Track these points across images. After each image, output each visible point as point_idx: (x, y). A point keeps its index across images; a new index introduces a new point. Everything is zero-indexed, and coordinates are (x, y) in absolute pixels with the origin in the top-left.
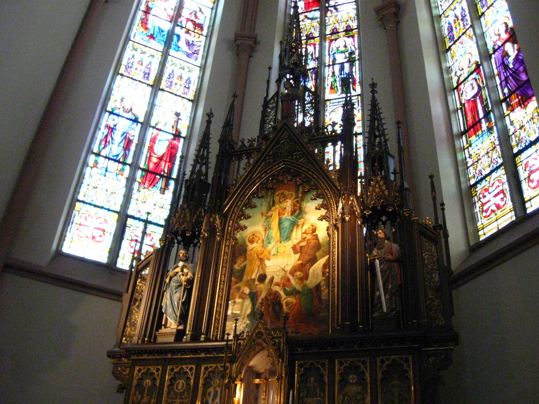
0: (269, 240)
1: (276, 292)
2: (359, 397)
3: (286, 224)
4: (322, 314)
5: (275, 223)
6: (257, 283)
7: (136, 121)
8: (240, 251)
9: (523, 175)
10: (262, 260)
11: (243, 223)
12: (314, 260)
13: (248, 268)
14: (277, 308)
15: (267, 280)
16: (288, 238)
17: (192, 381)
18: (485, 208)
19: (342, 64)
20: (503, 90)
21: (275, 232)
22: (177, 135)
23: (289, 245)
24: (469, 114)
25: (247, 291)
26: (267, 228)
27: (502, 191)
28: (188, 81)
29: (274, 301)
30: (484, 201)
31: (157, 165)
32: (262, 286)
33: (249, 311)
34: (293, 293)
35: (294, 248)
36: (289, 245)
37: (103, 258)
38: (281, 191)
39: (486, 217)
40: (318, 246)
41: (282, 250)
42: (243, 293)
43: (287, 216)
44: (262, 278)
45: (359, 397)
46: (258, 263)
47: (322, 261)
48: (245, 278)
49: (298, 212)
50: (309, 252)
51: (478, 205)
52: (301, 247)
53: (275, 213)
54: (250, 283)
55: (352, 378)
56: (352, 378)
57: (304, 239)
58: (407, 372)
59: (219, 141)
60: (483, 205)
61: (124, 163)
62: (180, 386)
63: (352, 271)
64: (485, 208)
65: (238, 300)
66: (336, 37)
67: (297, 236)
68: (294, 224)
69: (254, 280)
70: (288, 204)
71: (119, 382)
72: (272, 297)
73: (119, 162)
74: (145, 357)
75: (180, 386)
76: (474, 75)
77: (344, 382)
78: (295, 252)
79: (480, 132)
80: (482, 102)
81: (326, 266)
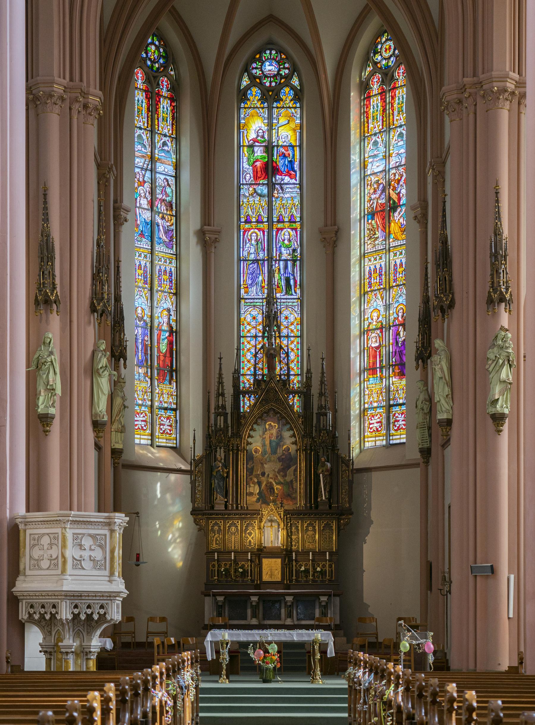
1: (271, 483)
2: (313, 536)
4: (294, 495)
6: (260, 476)
9: (392, 421)
10: (262, 464)
13: (255, 467)
14: (272, 490)
15: (266, 476)
17: (239, 527)
18: (371, 426)
19: (286, 261)
20: (392, 359)
24: (371, 359)
25: (256, 481)
27: (380, 422)
28: (171, 272)
30: (371, 422)
32: (263, 478)
33: (258, 491)
35: (279, 458)
38: (270, 423)
39: (370, 432)
41: (272, 459)
42: (254, 481)
45: (313, 536)
46: (260, 465)
48: (254, 473)
51: (367, 423)
52: (283, 459)
56: (310, 528)
57: (283, 454)
58: (332, 527)
59: (233, 387)
60: (370, 424)
62: (233, 530)
64: (371, 426)
65: (252, 485)
66: (282, 227)
69: (259, 475)
71: (198, 527)
72: (269, 485)
74: (220, 516)
75: (233, 530)
76: (378, 332)
77: (307, 530)
78: (280, 461)
79: (375, 376)
80: (380, 358)
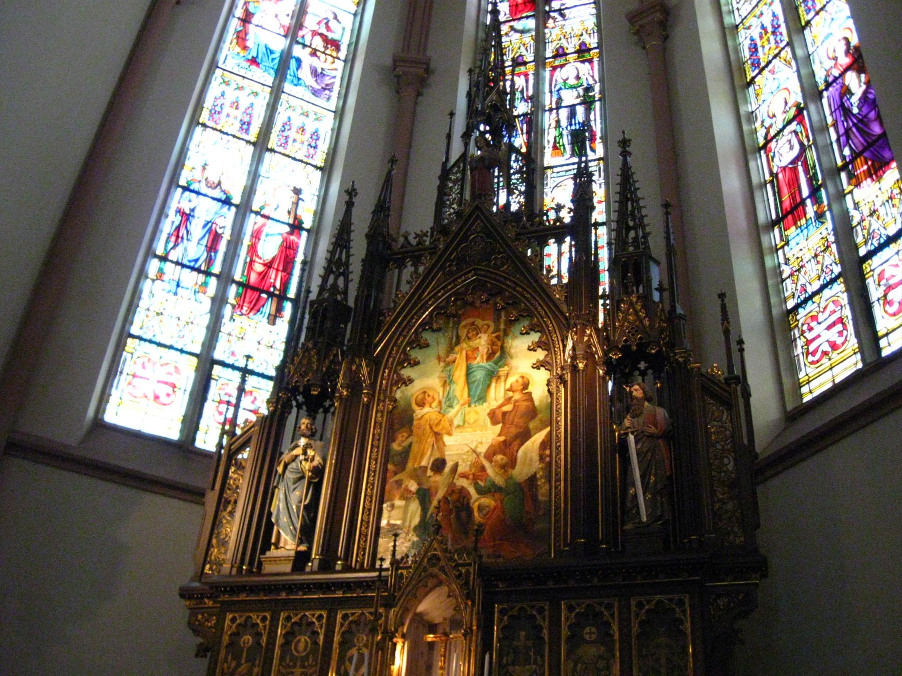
0: (449, 401)
1: (462, 489)
2: (601, 664)
3: (479, 375)
4: (539, 526)
5: (460, 374)
6: (429, 473)
7: (227, 202)
8: (401, 419)
9: (875, 293)
10: (438, 435)
11: (406, 372)
12: (525, 435)
13: (415, 448)
14: (463, 515)
15: (447, 469)
16: (482, 398)
17: (321, 637)
18: (812, 348)
19: (572, 108)
20: (841, 151)
21: (459, 388)
22: (296, 226)
23: (483, 409)
24: (785, 190)
25: (413, 486)
26: (447, 382)
27: (840, 320)
28: (315, 135)
29: (458, 503)
30: (810, 336)
31: (263, 276)
32: (438, 478)
33: (416, 521)
34: (490, 490)
35: (492, 415)
36: (483, 409)
37: (172, 432)
38: (470, 320)
39: (812, 363)
40: (532, 412)
41: (471, 418)
42: (407, 490)
43: (480, 361)
44: (439, 465)
45: (601, 664)
46: (431, 440)
47: (539, 437)
48: (410, 465)
49: (499, 354)
50: (518, 422)
51: (800, 342)
52: (504, 414)
53: (460, 357)
54: (418, 474)
55: (590, 632)
56: (590, 632)
57: (508, 400)
58: (681, 622)
59: (367, 236)
60: (808, 342)
61: (208, 274)
62: (301, 646)
63: (590, 454)
64: (812, 348)
65: (398, 503)
66: (563, 62)
67: (497, 395)
68: (492, 375)
69: (425, 468)
70: (482, 342)
71: (200, 640)
72: (455, 497)
73: (199, 270)
75: (301, 646)
76: (794, 126)
77: (575, 639)
78: (494, 422)
79: (803, 221)
80: (806, 171)
81: (545, 444)
